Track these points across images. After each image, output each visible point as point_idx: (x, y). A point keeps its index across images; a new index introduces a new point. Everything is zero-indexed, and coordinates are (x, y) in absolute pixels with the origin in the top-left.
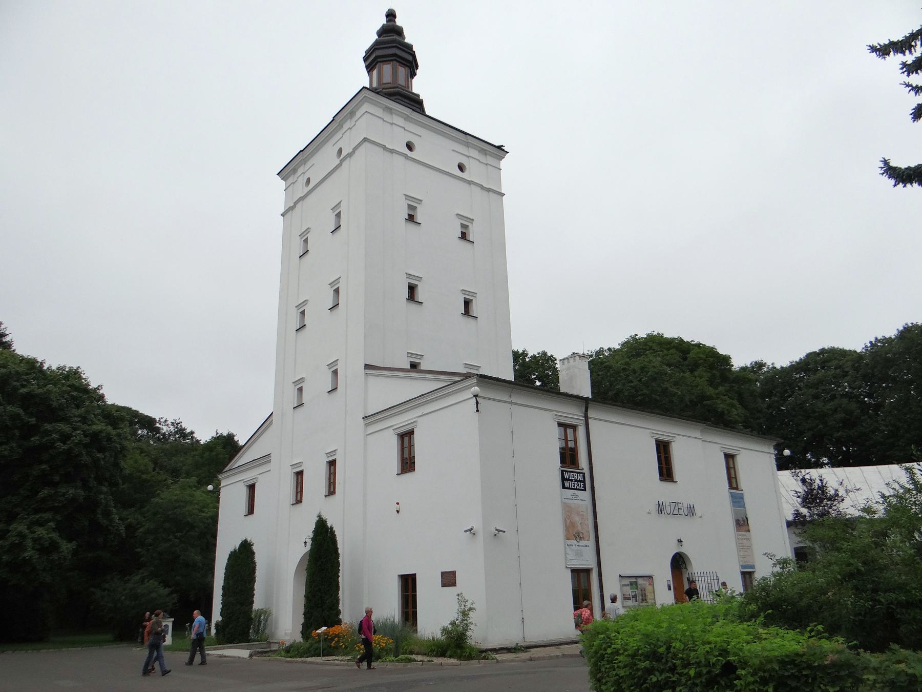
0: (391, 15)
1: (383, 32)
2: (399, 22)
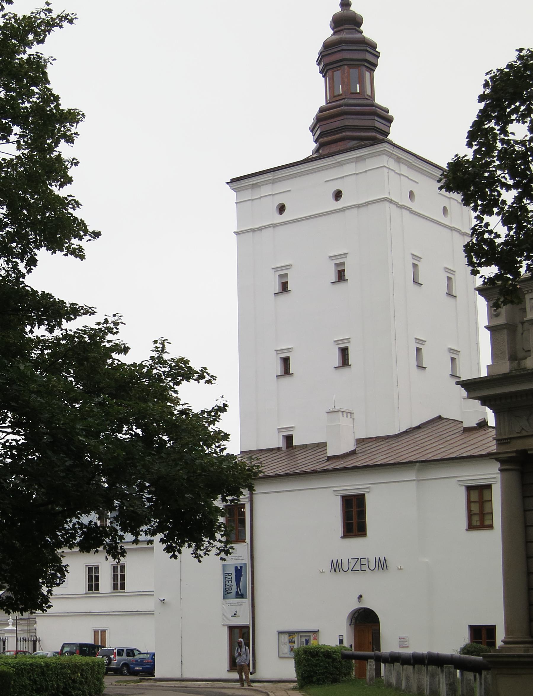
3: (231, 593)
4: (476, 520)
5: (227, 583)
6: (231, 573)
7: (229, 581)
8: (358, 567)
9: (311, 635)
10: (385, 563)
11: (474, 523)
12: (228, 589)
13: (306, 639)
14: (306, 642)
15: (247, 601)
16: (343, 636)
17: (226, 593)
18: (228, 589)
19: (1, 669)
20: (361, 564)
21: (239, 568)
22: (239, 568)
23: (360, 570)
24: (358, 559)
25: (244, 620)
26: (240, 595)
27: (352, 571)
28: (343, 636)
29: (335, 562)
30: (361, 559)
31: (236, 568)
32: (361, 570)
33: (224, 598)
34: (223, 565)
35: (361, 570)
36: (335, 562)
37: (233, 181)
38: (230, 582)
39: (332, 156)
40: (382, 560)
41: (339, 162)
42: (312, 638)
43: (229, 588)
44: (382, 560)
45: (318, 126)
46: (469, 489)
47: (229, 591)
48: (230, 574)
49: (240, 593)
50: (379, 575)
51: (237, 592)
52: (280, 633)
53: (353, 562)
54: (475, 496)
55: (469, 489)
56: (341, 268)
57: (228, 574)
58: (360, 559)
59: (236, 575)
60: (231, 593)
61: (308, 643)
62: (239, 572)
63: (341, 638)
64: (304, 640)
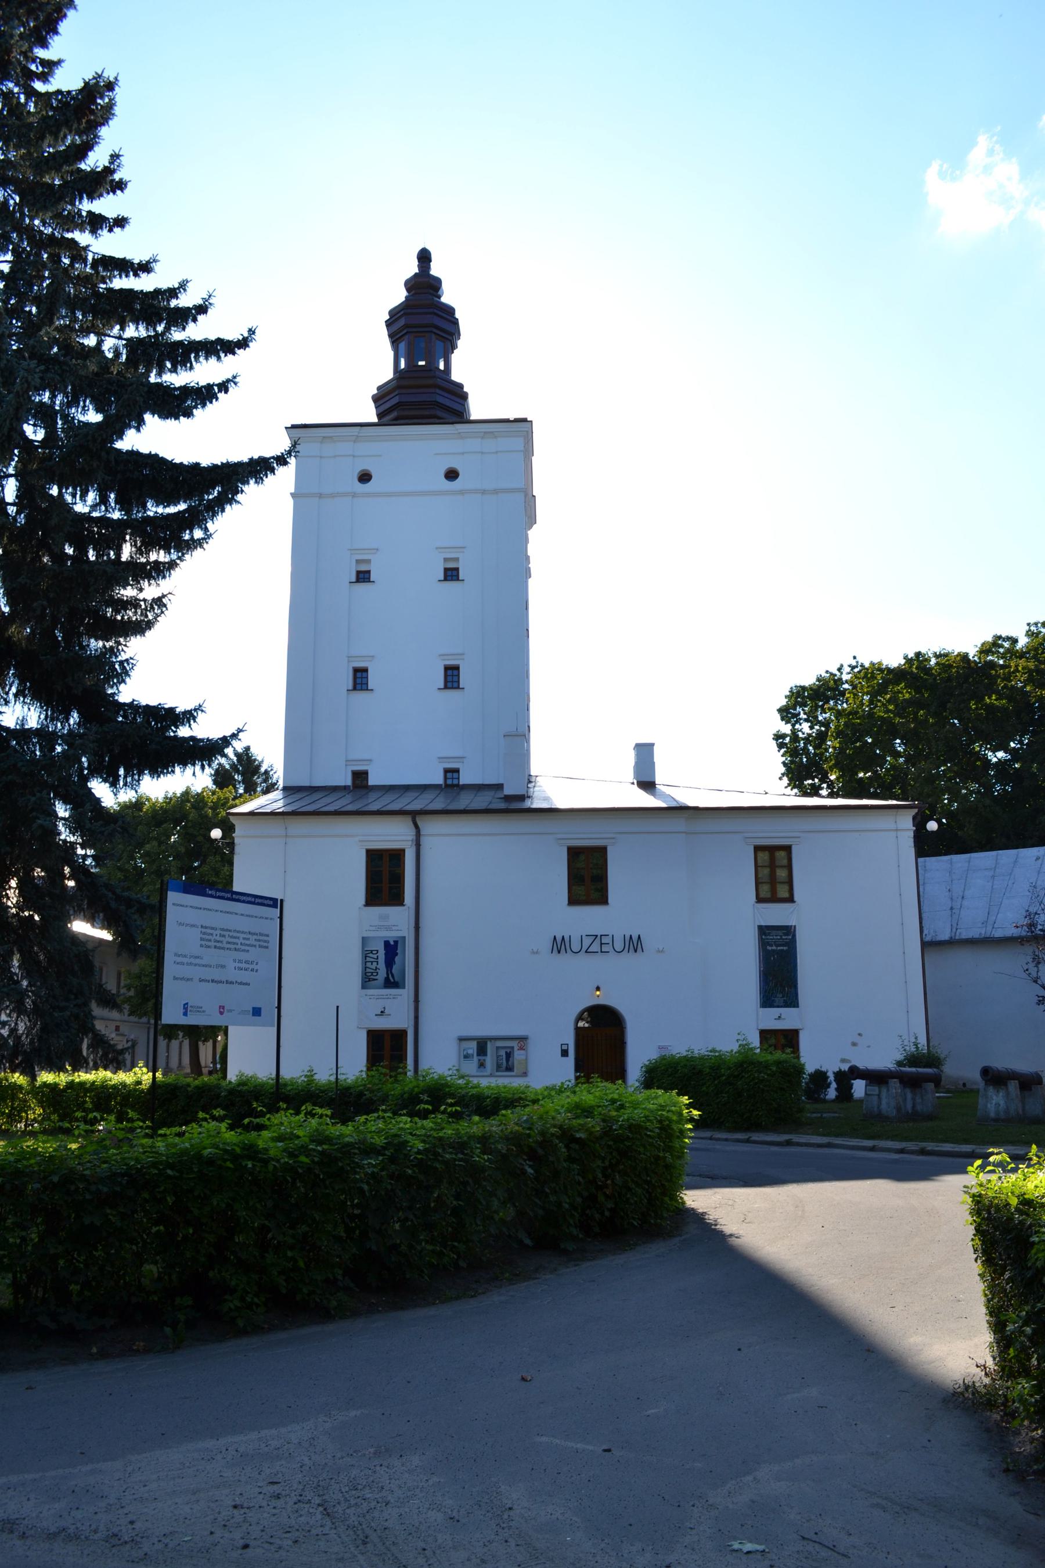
0: (424, 257)
1: (412, 285)
2: (435, 270)
3: (377, 980)
4: (765, 890)
5: (369, 964)
6: (377, 951)
7: (372, 962)
8: (595, 947)
9: (514, 1044)
10: (639, 943)
11: (786, 895)
12: (370, 974)
13: (506, 1052)
14: (506, 1057)
15: (405, 995)
16: (568, 1044)
17: (367, 980)
18: (370, 974)
19: (3, 1160)
20: (601, 944)
21: (392, 943)
22: (392, 943)
23: (599, 951)
24: (597, 936)
25: (398, 1019)
26: (391, 983)
27: (586, 952)
28: (568, 1044)
29: (559, 939)
30: (601, 936)
31: (387, 944)
32: (601, 952)
33: (364, 987)
34: (363, 938)
35: (601, 952)
36: (559, 939)
37: (294, 427)
38: (375, 964)
39: (453, 423)
40: (635, 939)
41: (459, 433)
42: (516, 1049)
43: (372, 973)
44: (635, 939)
45: (396, 393)
46: (757, 849)
47: (372, 977)
48: (374, 952)
49: (392, 980)
50: (629, 959)
51: (387, 979)
52: (461, 1039)
53: (587, 942)
54: (764, 856)
55: (757, 849)
56: (363, 568)
57: (372, 951)
58: (599, 937)
59: (385, 954)
60: (377, 980)
61: (510, 1057)
62: (392, 949)
63: (564, 1047)
64: (503, 1053)
